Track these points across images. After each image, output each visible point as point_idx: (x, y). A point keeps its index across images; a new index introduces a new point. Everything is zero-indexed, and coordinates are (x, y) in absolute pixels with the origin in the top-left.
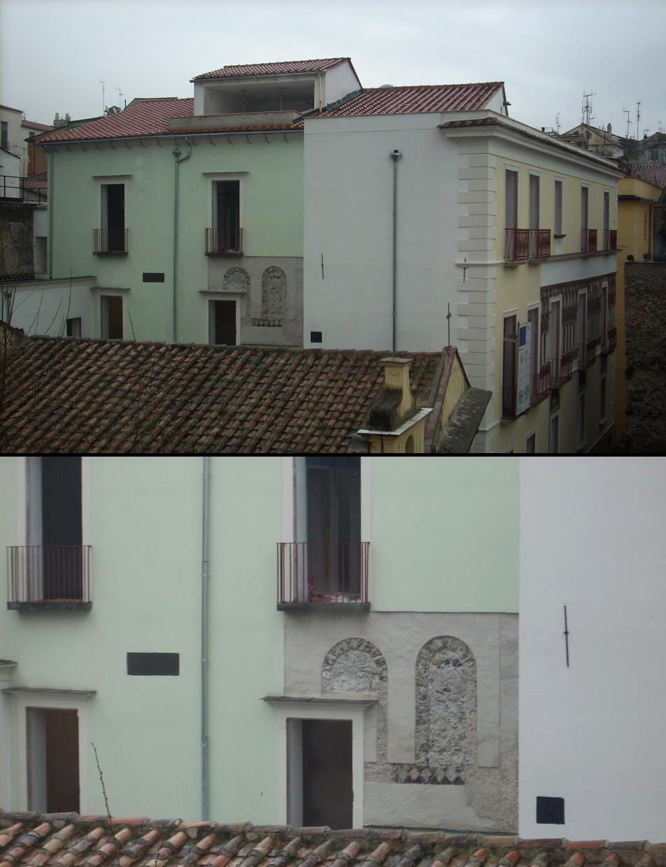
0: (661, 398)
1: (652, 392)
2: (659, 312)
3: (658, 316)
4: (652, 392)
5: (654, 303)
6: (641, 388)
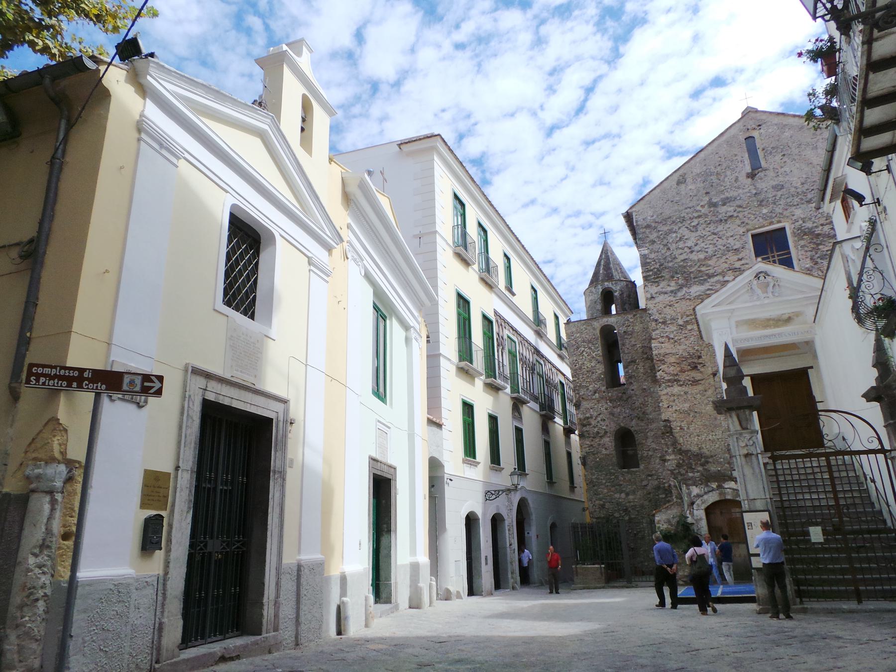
0: (604, 420)
1: (596, 417)
2: (594, 354)
3: (593, 357)
4: (596, 417)
5: (590, 348)
6: (588, 415)
